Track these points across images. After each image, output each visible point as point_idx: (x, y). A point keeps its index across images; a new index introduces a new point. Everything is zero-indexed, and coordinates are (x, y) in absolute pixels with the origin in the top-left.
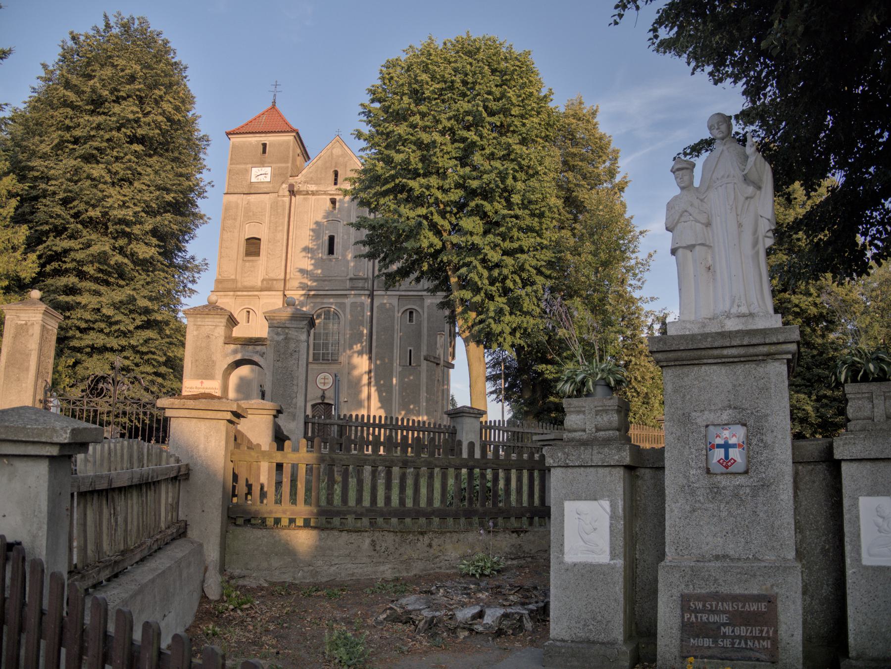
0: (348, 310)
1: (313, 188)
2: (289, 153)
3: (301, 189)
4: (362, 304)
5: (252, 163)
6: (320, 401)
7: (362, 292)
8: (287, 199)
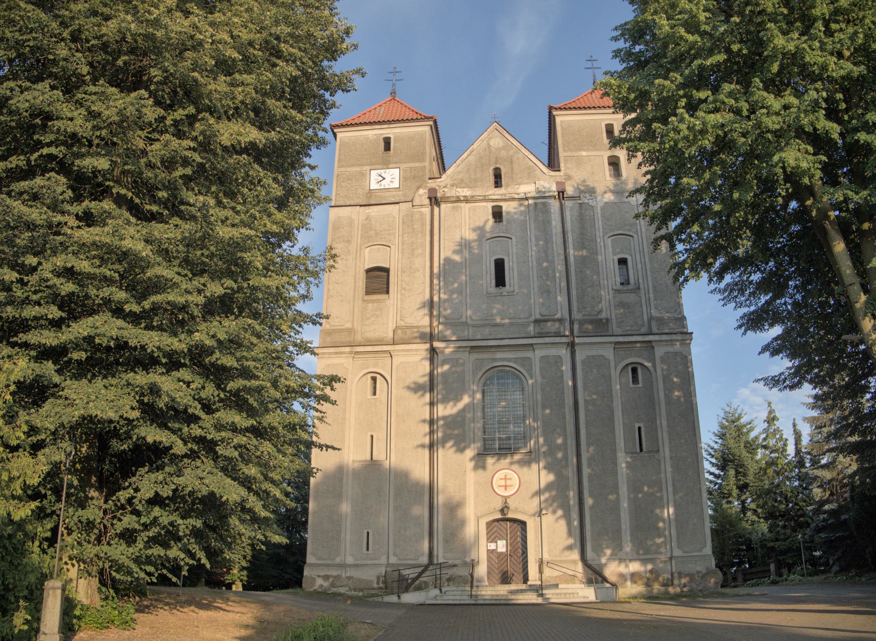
0: (537, 369)
1: (465, 192)
2: (425, 148)
4: (558, 360)
5: (371, 164)
6: (499, 516)
7: (558, 340)
8: (427, 210)
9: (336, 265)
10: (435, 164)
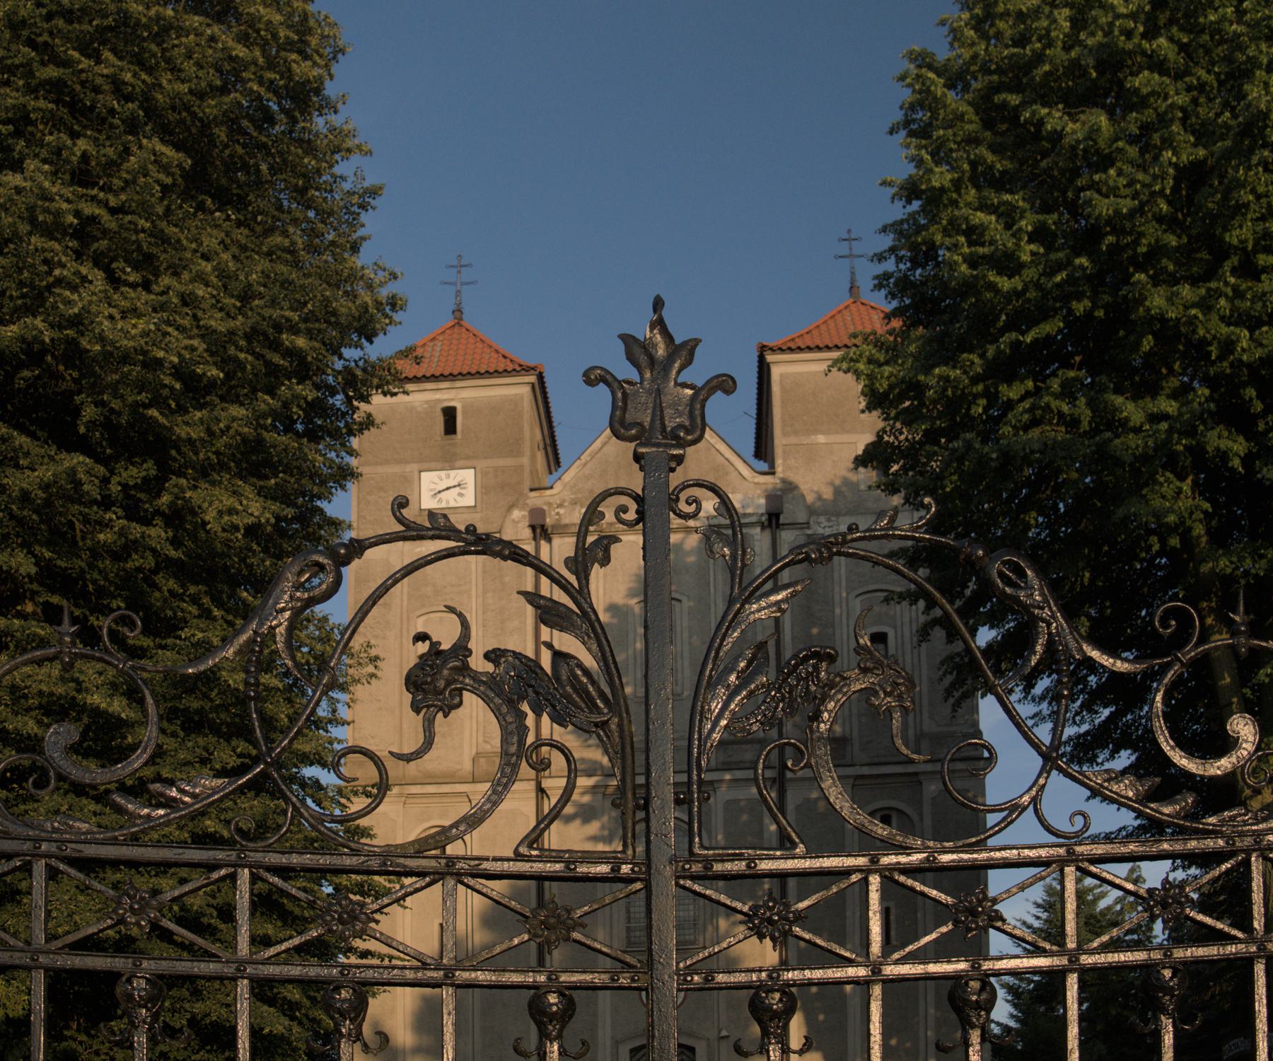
3: (566, 521)
9: (379, 674)
10: (540, 456)
